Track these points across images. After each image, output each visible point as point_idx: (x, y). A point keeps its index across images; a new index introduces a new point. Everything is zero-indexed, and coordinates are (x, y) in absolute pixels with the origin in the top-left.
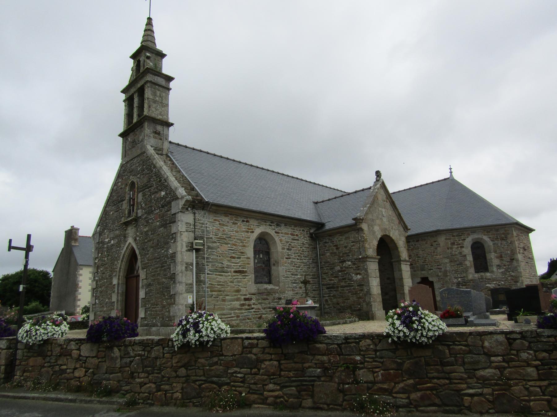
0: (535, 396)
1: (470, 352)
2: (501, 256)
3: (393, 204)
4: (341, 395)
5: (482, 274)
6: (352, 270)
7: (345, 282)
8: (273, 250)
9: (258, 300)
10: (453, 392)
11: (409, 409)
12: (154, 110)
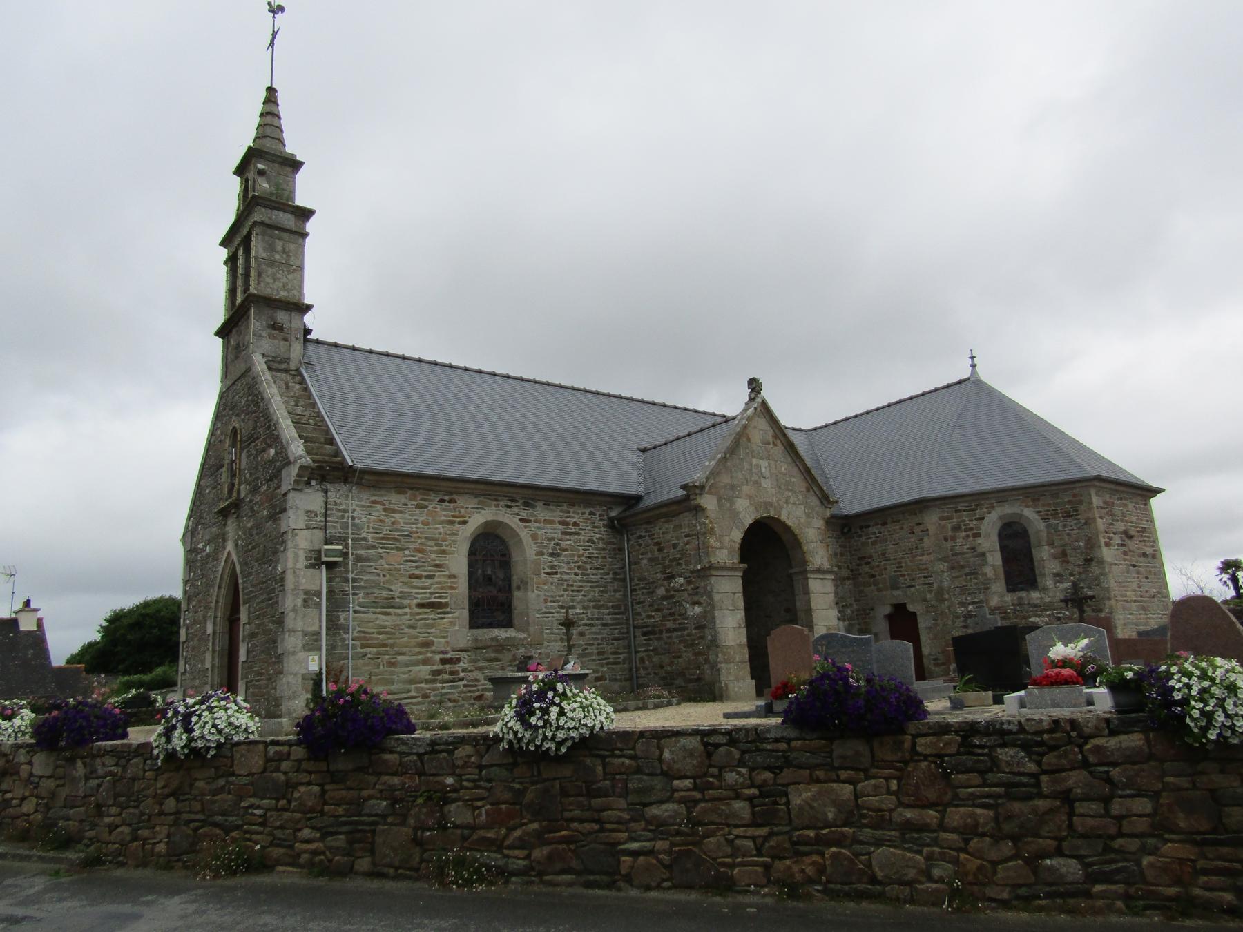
0: (744, 856)
1: (638, 770)
2: (1064, 554)
3: (790, 447)
4: (418, 849)
5: (1023, 594)
6: (685, 594)
7: (675, 620)
8: (516, 557)
9: (475, 661)
10: (602, 847)
11: (526, 878)
12: (269, 280)
